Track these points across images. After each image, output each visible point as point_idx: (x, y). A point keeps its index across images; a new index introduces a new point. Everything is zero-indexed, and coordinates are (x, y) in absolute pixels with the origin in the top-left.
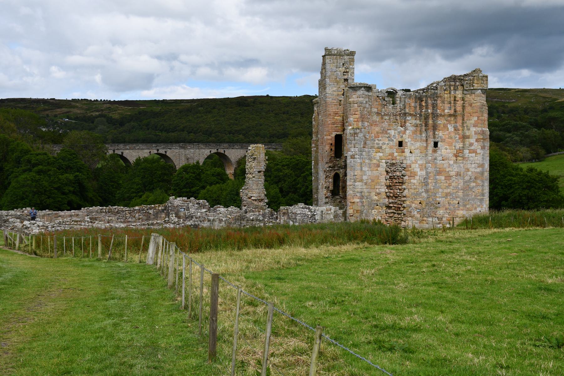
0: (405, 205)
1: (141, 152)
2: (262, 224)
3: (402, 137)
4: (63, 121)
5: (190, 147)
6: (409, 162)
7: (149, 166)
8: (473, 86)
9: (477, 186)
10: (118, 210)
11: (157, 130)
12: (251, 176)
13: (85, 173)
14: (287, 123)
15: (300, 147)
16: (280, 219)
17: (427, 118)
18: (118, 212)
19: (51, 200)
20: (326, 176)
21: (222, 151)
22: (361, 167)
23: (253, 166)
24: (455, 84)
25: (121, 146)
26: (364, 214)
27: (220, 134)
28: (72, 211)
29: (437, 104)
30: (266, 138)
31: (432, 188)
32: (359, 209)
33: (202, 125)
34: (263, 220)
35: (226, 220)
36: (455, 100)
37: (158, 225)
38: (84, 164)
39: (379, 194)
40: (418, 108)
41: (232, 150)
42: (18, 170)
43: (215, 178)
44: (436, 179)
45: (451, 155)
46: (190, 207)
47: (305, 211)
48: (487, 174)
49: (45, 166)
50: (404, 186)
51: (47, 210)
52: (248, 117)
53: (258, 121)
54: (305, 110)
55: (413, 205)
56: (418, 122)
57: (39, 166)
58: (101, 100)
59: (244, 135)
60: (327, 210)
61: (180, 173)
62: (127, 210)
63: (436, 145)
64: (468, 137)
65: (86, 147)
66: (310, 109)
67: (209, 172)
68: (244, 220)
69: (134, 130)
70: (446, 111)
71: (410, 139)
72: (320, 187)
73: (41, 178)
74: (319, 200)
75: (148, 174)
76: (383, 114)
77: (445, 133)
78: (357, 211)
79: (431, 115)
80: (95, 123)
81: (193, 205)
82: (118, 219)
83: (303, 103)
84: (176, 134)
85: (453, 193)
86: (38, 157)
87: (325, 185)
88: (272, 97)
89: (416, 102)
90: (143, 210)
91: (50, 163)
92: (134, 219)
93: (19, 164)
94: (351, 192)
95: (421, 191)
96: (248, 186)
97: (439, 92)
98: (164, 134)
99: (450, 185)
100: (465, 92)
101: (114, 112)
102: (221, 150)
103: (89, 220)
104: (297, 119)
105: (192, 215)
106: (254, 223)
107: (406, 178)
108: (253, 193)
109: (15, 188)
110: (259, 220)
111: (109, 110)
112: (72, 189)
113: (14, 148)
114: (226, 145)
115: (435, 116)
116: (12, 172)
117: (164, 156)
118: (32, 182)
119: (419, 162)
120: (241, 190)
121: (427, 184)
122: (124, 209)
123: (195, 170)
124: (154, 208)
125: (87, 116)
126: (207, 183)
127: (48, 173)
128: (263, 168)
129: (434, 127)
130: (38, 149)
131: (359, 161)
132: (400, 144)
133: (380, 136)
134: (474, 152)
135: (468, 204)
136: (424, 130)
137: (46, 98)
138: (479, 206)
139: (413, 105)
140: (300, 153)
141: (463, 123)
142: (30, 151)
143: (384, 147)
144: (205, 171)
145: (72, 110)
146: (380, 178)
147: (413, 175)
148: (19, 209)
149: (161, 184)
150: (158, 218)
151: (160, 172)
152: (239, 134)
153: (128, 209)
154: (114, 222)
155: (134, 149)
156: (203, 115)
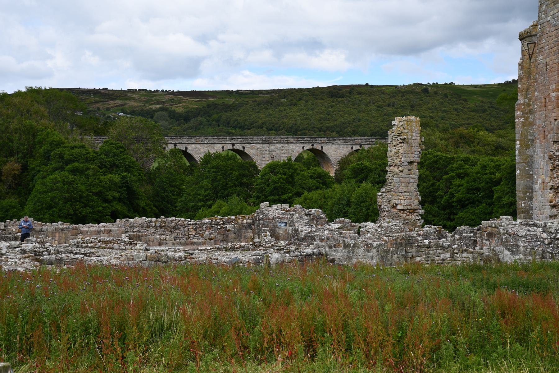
1: (211, 148)
5: (275, 142)
10: (176, 224)
12: (396, 170)
16: (482, 245)
18: (175, 228)
19: (89, 210)
20: (554, 167)
21: (318, 147)
23: (400, 152)
25: (185, 139)
28: (101, 224)
33: (285, 120)
34: (450, 246)
35: (380, 245)
37: (243, 250)
38: (134, 162)
41: (332, 145)
43: (314, 181)
46: (295, 220)
47: (535, 231)
49: (82, 163)
51: (60, 222)
53: (355, 115)
57: (75, 164)
58: (163, 91)
61: (265, 174)
62: (190, 224)
65: (138, 139)
66: (422, 100)
67: (305, 173)
68: (411, 247)
69: (202, 126)
72: (537, 187)
73: (75, 178)
75: (221, 175)
80: (155, 117)
81: (301, 218)
82: (175, 239)
84: (253, 132)
86: (73, 151)
87: (551, 184)
88: (372, 86)
90: (217, 225)
91: (89, 159)
92: (202, 240)
93: (49, 160)
96: (392, 187)
101: (178, 105)
102: (318, 145)
103: (127, 239)
104: (406, 112)
105: (312, 234)
106: (431, 252)
108: (399, 199)
109: (40, 193)
110: (442, 246)
111: (172, 102)
112: (117, 195)
113: (43, 138)
114: (324, 139)
116: (39, 171)
117: (242, 153)
118: (64, 185)
120: (379, 194)
122: (186, 222)
124: (235, 221)
126: (303, 188)
127: (86, 173)
128: (417, 156)
130: (75, 140)
137: (97, 88)
142: (63, 143)
144: (300, 171)
145: (127, 102)
148: (14, 220)
149: (238, 189)
150: (241, 238)
151: (237, 173)
152: (331, 132)
153: (192, 223)
155: (202, 142)
156: (286, 108)
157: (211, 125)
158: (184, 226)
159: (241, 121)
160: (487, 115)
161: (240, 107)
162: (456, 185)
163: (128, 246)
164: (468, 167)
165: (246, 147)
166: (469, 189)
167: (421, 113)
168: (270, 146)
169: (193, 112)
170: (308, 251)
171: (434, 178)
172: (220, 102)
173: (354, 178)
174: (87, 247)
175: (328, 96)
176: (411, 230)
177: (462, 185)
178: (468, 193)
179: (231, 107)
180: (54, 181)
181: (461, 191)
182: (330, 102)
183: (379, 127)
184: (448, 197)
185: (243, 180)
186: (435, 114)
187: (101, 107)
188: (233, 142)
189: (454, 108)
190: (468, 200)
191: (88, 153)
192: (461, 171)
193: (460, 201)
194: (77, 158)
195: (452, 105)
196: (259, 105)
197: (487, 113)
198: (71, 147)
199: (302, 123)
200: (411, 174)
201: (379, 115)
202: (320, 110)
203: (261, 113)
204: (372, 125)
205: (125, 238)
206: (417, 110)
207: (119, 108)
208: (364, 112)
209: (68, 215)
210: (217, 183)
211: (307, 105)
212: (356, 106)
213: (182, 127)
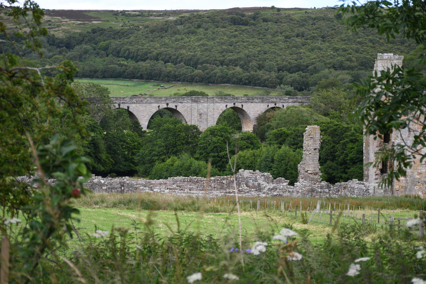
2: (328, 196)
5: (203, 101)
12: (308, 153)
14: (302, 51)
15: (331, 101)
16: (342, 192)
18: (197, 182)
21: (239, 105)
26: (408, 190)
27: (209, 65)
32: (404, 185)
33: (183, 51)
34: (329, 192)
43: (245, 142)
52: (247, 42)
54: (328, 32)
59: (242, 67)
61: (207, 136)
66: (335, 30)
69: (88, 55)
74: (370, 177)
75: (171, 136)
78: (402, 187)
83: (324, 19)
88: (279, 10)
92: (210, 188)
98: (131, 64)
101: (57, 29)
104: (317, 44)
111: (50, 25)
120: (299, 165)
122: (202, 179)
123: (223, 133)
124: (227, 179)
140: (332, 108)
149: (185, 147)
152: (235, 66)
156: (184, 36)
157: (98, 54)
158: (201, 181)
159: (133, 51)
160: (406, 47)
161: (131, 34)
162: (349, 148)
164: (358, 134)
166: (358, 151)
167: (333, 45)
169: (75, 38)
171: (334, 142)
172: (106, 26)
173: (275, 140)
175: (230, 23)
176: (315, 184)
177: (354, 148)
178: (357, 154)
179: (119, 34)
181: (353, 152)
182: (232, 31)
183: (287, 61)
184: (343, 156)
186: (348, 46)
188: (167, 101)
189: (369, 39)
190: (357, 159)
192: (353, 138)
193: (352, 159)
195: (368, 36)
197: (406, 44)
199: (202, 55)
200: (315, 155)
201: (287, 47)
202: (222, 40)
203: (155, 41)
204: (279, 59)
206: (329, 41)
208: (270, 43)
211: (207, 33)
212: (261, 36)
213: (65, 55)
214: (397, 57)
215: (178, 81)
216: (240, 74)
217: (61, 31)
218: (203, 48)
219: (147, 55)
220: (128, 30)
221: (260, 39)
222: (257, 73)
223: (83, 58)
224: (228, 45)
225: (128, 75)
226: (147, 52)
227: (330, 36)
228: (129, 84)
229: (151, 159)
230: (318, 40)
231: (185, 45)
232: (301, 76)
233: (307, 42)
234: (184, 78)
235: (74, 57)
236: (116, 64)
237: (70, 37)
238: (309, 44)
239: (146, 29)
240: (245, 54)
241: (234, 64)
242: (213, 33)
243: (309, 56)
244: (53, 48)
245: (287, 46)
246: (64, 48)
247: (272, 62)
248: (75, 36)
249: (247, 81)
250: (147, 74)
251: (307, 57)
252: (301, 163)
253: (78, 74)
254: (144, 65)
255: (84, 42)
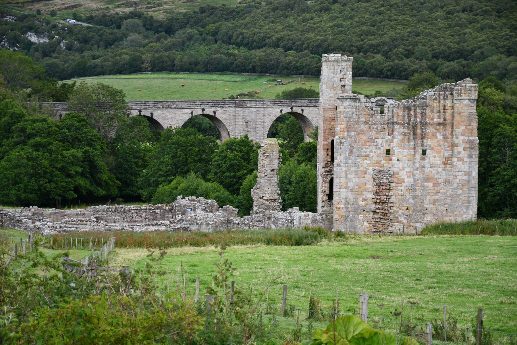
0: (391, 211)
3: (389, 145)
4: (67, 24)
5: (250, 105)
6: (396, 169)
7: (183, 139)
8: (461, 96)
9: (464, 193)
11: (230, 44)
12: (263, 175)
13: (98, 147)
14: (467, 30)
16: (265, 223)
17: (415, 127)
18: (124, 212)
19: (53, 185)
21: (298, 110)
22: (346, 175)
24: (445, 93)
29: (425, 113)
30: (424, 60)
31: (420, 194)
32: (344, 214)
33: (311, 35)
36: (444, 109)
39: (366, 200)
40: (406, 117)
42: (8, 142)
44: (424, 186)
45: (439, 163)
48: (475, 182)
49: (45, 137)
50: (391, 193)
52: (396, 20)
55: (400, 211)
56: (406, 131)
60: (305, 216)
61: (223, 151)
63: (424, 153)
64: (457, 146)
70: (435, 120)
71: (397, 148)
73: (39, 155)
76: (370, 123)
77: (434, 142)
78: (342, 216)
79: (419, 124)
80: (123, 27)
85: (442, 199)
86: (35, 125)
89: (404, 111)
91: (51, 133)
92: (140, 219)
94: (337, 198)
95: (408, 197)
97: (428, 101)
99: (438, 192)
100: (455, 101)
101: (157, 9)
102: (298, 108)
103: (94, 219)
107: (393, 185)
112: (80, 170)
114: (305, 101)
115: (423, 124)
118: (28, 161)
119: (406, 170)
121: (414, 191)
124: (162, 208)
125: (108, 14)
127: (48, 147)
129: (422, 135)
131: (344, 169)
132: (388, 152)
133: (368, 144)
134: (461, 160)
135: (456, 211)
136: (412, 138)
138: (465, 213)
139: (401, 114)
141: (452, 132)
142: (23, 116)
143: (371, 155)
146: (367, 185)
147: (401, 182)
154: (121, 221)
157: (204, 40)
158: (129, 211)
159: (248, 35)
163: (96, 224)
165: (217, 112)
168: (244, 110)
169: (178, 19)
170: (179, 226)
174: (72, 224)
179: (234, 13)
180: (19, 157)
182: (378, 6)
183: (445, 45)
185: (202, 156)
187: (43, 9)
188: (203, 106)
191: (49, 127)
194: (39, 132)
196: (274, 10)
198: (32, 120)
199: (334, 39)
200: (272, 177)
201: (447, 26)
202: (362, 19)
203: (277, 23)
204: (435, 42)
205: (93, 218)
206: (506, 17)
207: (69, 11)
208: (426, 21)
209: (33, 190)
210: (178, 159)
211: (344, 10)
212: (415, 12)
214: (345, 58)
215: (300, 74)
216: (380, 64)
217: (162, 11)
218: (336, 30)
219: (265, 40)
220: (245, 7)
221: (412, 16)
222: (403, 62)
223: (186, 45)
224: (371, 26)
225: (237, 67)
226: (266, 37)
227: (508, 9)
228: (237, 79)
229: (156, 181)
230: (491, 15)
231: (315, 26)
232: (461, 65)
233: (476, 19)
234: (308, 70)
235: (173, 45)
236: (223, 53)
237: (172, 18)
238: (478, 21)
239: (268, 7)
240: (390, 37)
241: (375, 51)
242: (352, 10)
243: (476, 38)
244: (150, 33)
245: (448, 24)
246: (163, 33)
247: (424, 47)
248: (178, 17)
249: (389, 73)
250: (261, 66)
251: (473, 39)
252: (254, 187)
253: (174, 68)
254: (257, 54)
255: (189, 25)
